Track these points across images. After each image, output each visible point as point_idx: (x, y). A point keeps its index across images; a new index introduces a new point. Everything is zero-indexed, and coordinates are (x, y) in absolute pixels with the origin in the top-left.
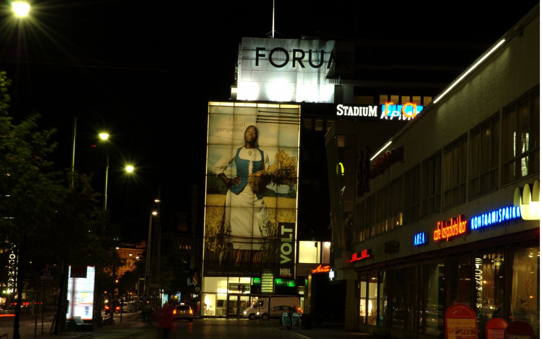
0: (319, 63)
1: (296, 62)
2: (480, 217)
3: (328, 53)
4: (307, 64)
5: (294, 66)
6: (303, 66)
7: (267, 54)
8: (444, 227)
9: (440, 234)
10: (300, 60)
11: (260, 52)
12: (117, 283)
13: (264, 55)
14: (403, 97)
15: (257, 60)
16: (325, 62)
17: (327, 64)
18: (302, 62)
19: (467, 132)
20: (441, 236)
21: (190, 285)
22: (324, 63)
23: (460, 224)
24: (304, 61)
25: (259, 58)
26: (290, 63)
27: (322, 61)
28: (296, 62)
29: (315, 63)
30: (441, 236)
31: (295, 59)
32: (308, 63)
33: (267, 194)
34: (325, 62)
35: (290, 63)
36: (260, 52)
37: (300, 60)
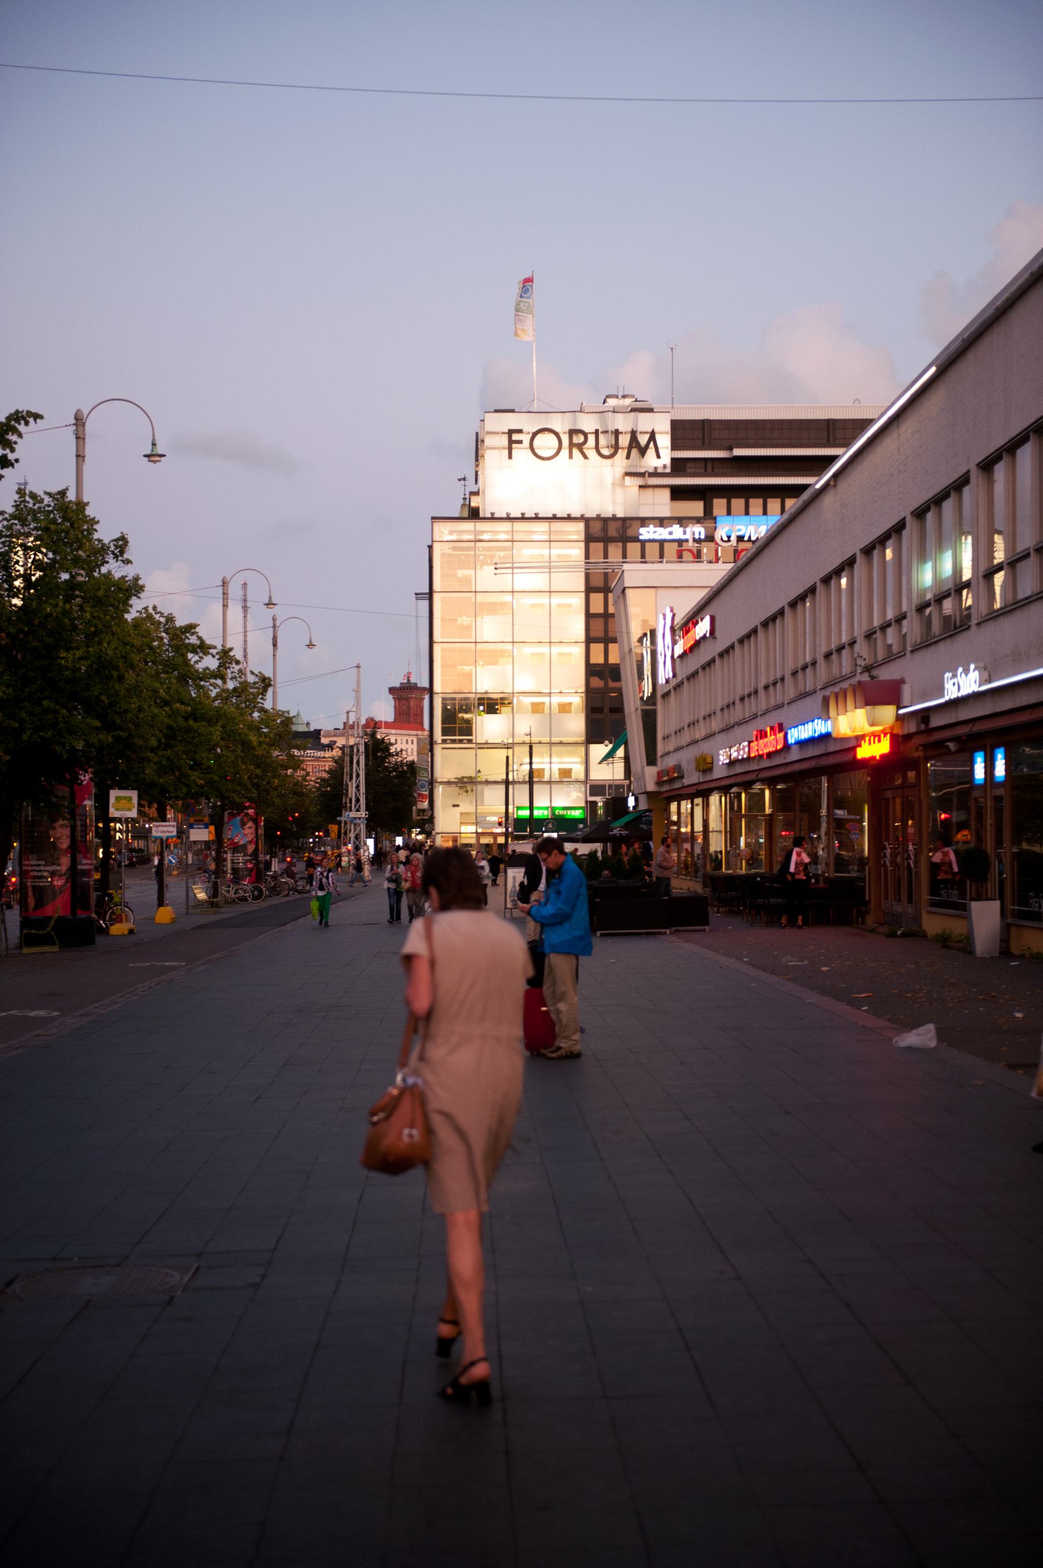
0: (612, 450)
1: (575, 451)
2: (676, 803)
3: (625, 433)
4: (592, 453)
5: (571, 457)
6: (585, 457)
7: (526, 438)
8: (761, 738)
9: (757, 748)
10: (580, 447)
11: (515, 437)
12: (279, 835)
13: (520, 442)
14: (769, 500)
15: (510, 449)
16: (622, 448)
17: (626, 450)
18: (584, 450)
19: (855, 554)
20: (758, 750)
21: (418, 820)
22: (620, 451)
23: (778, 735)
24: (588, 449)
25: (514, 446)
26: (565, 452)
27: (616, 447)
28: (634, 452)
29: (606, 452)
30: (758, 750)
31: (572, 445)
32: (594, 451)
33: (124, 785)
34: (622, 448)
35: (565, 452)
36: (515, 437)
37: (580, 447)
